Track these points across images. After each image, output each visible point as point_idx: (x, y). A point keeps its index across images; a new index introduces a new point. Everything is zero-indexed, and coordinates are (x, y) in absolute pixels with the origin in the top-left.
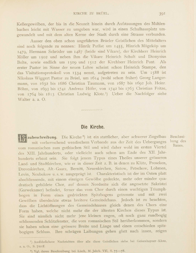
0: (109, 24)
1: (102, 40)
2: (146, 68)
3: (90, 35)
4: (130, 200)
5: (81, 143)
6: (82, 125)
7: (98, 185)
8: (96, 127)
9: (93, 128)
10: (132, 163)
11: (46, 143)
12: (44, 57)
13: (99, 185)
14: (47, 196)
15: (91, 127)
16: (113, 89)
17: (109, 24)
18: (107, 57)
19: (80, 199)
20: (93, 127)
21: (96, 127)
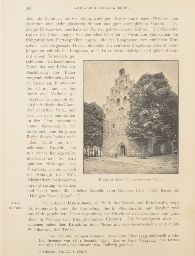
0: (31, 94)
1: (123, 202)
3: (28, 89)
4: (73, 170)
5: (29, 62)
7: (63, 186)
11: (58, 94)
12: (154, 191)
13: (64, 186)
14: (134, 35)
17: (31, 94)
19: (33, 136)
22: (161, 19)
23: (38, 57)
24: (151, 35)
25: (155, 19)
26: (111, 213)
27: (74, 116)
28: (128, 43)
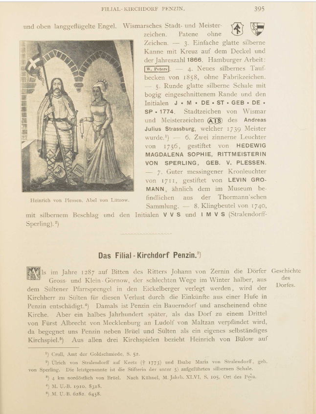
2: (245, 331)
6: (99, 253)
8: (146, 256)
9: (141, 256)
10: (61, 298)
15: (139, 255)
16: (170, 111)
18: (193, 340)
20: (141, 255)
21: (146, 256)
22: (211, 43)
23: (170, 95)
24: (211, 61)
25: (213, 281)
26: (186, 102)
27: (263, 112)
28: (230, 318)
